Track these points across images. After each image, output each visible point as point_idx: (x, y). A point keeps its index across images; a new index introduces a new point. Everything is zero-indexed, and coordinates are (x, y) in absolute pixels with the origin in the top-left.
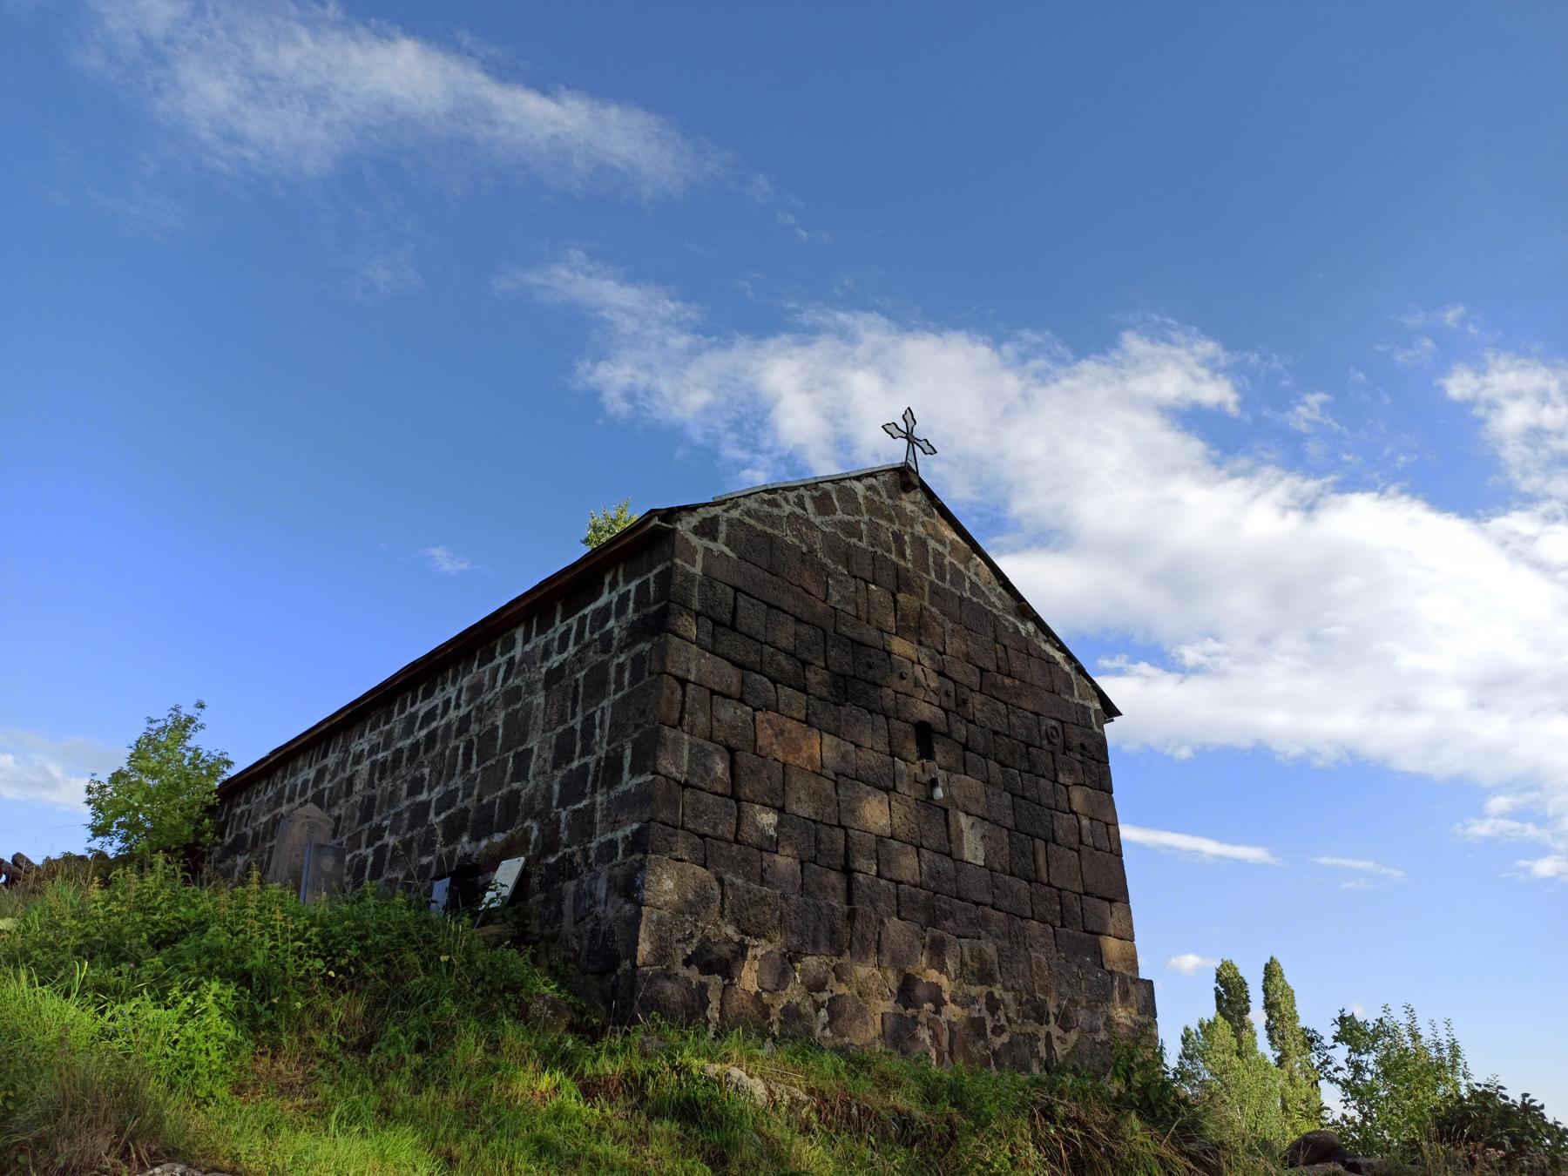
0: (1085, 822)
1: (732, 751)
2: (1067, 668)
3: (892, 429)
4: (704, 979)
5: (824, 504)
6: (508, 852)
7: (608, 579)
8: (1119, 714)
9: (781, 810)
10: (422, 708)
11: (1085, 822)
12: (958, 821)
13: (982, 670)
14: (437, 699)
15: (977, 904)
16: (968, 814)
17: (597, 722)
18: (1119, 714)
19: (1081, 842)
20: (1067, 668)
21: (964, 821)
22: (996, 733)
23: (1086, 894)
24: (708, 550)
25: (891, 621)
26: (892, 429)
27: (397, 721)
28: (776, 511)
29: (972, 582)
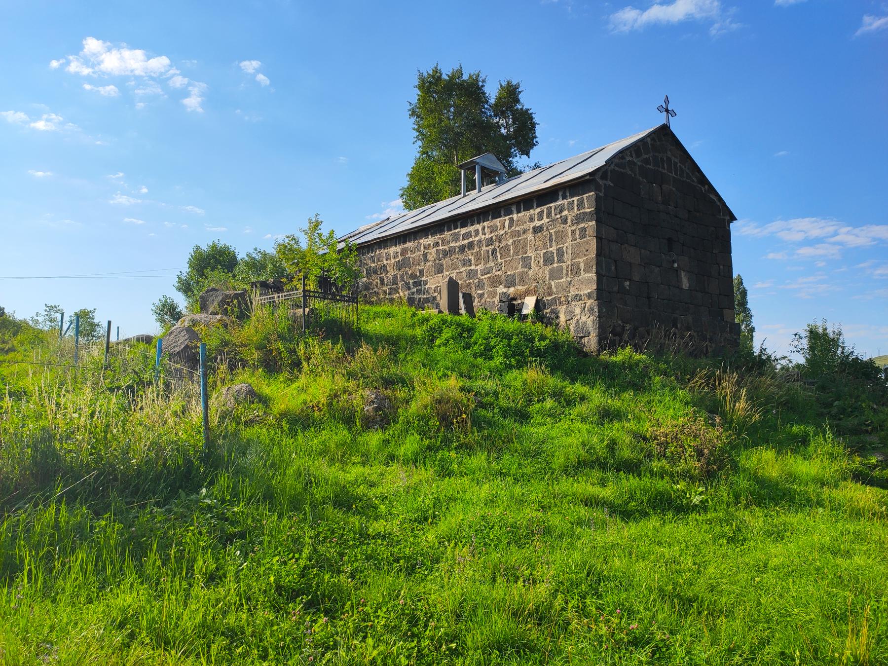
0: (721, 267)
1: (615, 261)
2: (719, 204)
3: (674, 114)
4: (614, 338)
5: (638, 154)
6: (528, 293)
7: (560, 194)
8: (736, 219)
9: (630, 280)
10: (463, 231)
11: (721, 267)
12: (681, 275)
13: (689, 211)
14: (471, 229)
15: (686, 303)
16: (684, 271)
17: (565, 251)
18: (736, 219)
19: (719, 275)
20: (719, 204)
21: (683, 274)
22: (693, 237)
23: (720, 294)
24: (605, 185)
25: (660, 198)
26: (674, 114)
27: (447, 235)
28: (624, 161)
29: (686, 173)
